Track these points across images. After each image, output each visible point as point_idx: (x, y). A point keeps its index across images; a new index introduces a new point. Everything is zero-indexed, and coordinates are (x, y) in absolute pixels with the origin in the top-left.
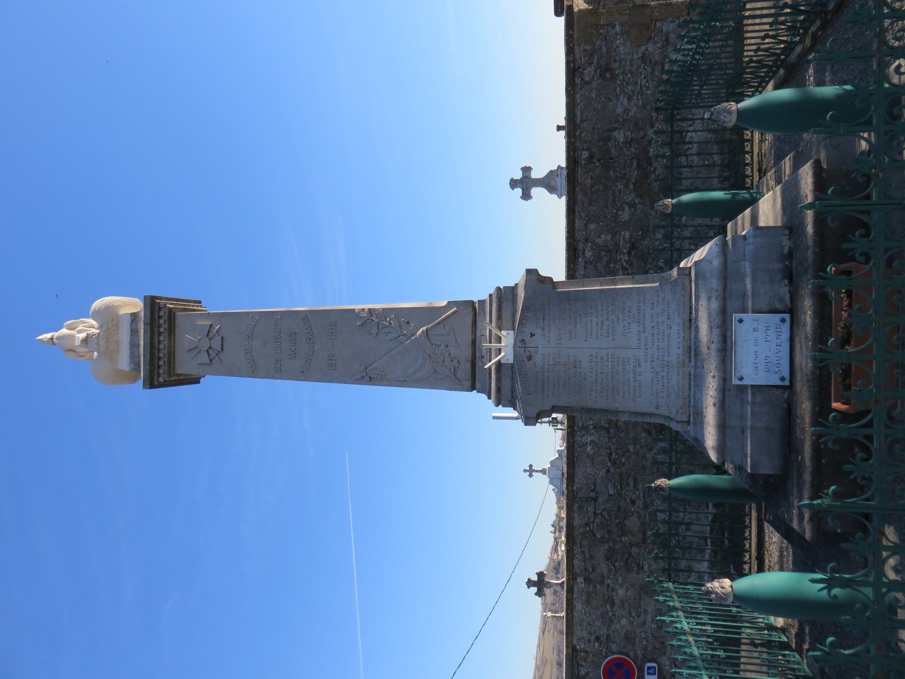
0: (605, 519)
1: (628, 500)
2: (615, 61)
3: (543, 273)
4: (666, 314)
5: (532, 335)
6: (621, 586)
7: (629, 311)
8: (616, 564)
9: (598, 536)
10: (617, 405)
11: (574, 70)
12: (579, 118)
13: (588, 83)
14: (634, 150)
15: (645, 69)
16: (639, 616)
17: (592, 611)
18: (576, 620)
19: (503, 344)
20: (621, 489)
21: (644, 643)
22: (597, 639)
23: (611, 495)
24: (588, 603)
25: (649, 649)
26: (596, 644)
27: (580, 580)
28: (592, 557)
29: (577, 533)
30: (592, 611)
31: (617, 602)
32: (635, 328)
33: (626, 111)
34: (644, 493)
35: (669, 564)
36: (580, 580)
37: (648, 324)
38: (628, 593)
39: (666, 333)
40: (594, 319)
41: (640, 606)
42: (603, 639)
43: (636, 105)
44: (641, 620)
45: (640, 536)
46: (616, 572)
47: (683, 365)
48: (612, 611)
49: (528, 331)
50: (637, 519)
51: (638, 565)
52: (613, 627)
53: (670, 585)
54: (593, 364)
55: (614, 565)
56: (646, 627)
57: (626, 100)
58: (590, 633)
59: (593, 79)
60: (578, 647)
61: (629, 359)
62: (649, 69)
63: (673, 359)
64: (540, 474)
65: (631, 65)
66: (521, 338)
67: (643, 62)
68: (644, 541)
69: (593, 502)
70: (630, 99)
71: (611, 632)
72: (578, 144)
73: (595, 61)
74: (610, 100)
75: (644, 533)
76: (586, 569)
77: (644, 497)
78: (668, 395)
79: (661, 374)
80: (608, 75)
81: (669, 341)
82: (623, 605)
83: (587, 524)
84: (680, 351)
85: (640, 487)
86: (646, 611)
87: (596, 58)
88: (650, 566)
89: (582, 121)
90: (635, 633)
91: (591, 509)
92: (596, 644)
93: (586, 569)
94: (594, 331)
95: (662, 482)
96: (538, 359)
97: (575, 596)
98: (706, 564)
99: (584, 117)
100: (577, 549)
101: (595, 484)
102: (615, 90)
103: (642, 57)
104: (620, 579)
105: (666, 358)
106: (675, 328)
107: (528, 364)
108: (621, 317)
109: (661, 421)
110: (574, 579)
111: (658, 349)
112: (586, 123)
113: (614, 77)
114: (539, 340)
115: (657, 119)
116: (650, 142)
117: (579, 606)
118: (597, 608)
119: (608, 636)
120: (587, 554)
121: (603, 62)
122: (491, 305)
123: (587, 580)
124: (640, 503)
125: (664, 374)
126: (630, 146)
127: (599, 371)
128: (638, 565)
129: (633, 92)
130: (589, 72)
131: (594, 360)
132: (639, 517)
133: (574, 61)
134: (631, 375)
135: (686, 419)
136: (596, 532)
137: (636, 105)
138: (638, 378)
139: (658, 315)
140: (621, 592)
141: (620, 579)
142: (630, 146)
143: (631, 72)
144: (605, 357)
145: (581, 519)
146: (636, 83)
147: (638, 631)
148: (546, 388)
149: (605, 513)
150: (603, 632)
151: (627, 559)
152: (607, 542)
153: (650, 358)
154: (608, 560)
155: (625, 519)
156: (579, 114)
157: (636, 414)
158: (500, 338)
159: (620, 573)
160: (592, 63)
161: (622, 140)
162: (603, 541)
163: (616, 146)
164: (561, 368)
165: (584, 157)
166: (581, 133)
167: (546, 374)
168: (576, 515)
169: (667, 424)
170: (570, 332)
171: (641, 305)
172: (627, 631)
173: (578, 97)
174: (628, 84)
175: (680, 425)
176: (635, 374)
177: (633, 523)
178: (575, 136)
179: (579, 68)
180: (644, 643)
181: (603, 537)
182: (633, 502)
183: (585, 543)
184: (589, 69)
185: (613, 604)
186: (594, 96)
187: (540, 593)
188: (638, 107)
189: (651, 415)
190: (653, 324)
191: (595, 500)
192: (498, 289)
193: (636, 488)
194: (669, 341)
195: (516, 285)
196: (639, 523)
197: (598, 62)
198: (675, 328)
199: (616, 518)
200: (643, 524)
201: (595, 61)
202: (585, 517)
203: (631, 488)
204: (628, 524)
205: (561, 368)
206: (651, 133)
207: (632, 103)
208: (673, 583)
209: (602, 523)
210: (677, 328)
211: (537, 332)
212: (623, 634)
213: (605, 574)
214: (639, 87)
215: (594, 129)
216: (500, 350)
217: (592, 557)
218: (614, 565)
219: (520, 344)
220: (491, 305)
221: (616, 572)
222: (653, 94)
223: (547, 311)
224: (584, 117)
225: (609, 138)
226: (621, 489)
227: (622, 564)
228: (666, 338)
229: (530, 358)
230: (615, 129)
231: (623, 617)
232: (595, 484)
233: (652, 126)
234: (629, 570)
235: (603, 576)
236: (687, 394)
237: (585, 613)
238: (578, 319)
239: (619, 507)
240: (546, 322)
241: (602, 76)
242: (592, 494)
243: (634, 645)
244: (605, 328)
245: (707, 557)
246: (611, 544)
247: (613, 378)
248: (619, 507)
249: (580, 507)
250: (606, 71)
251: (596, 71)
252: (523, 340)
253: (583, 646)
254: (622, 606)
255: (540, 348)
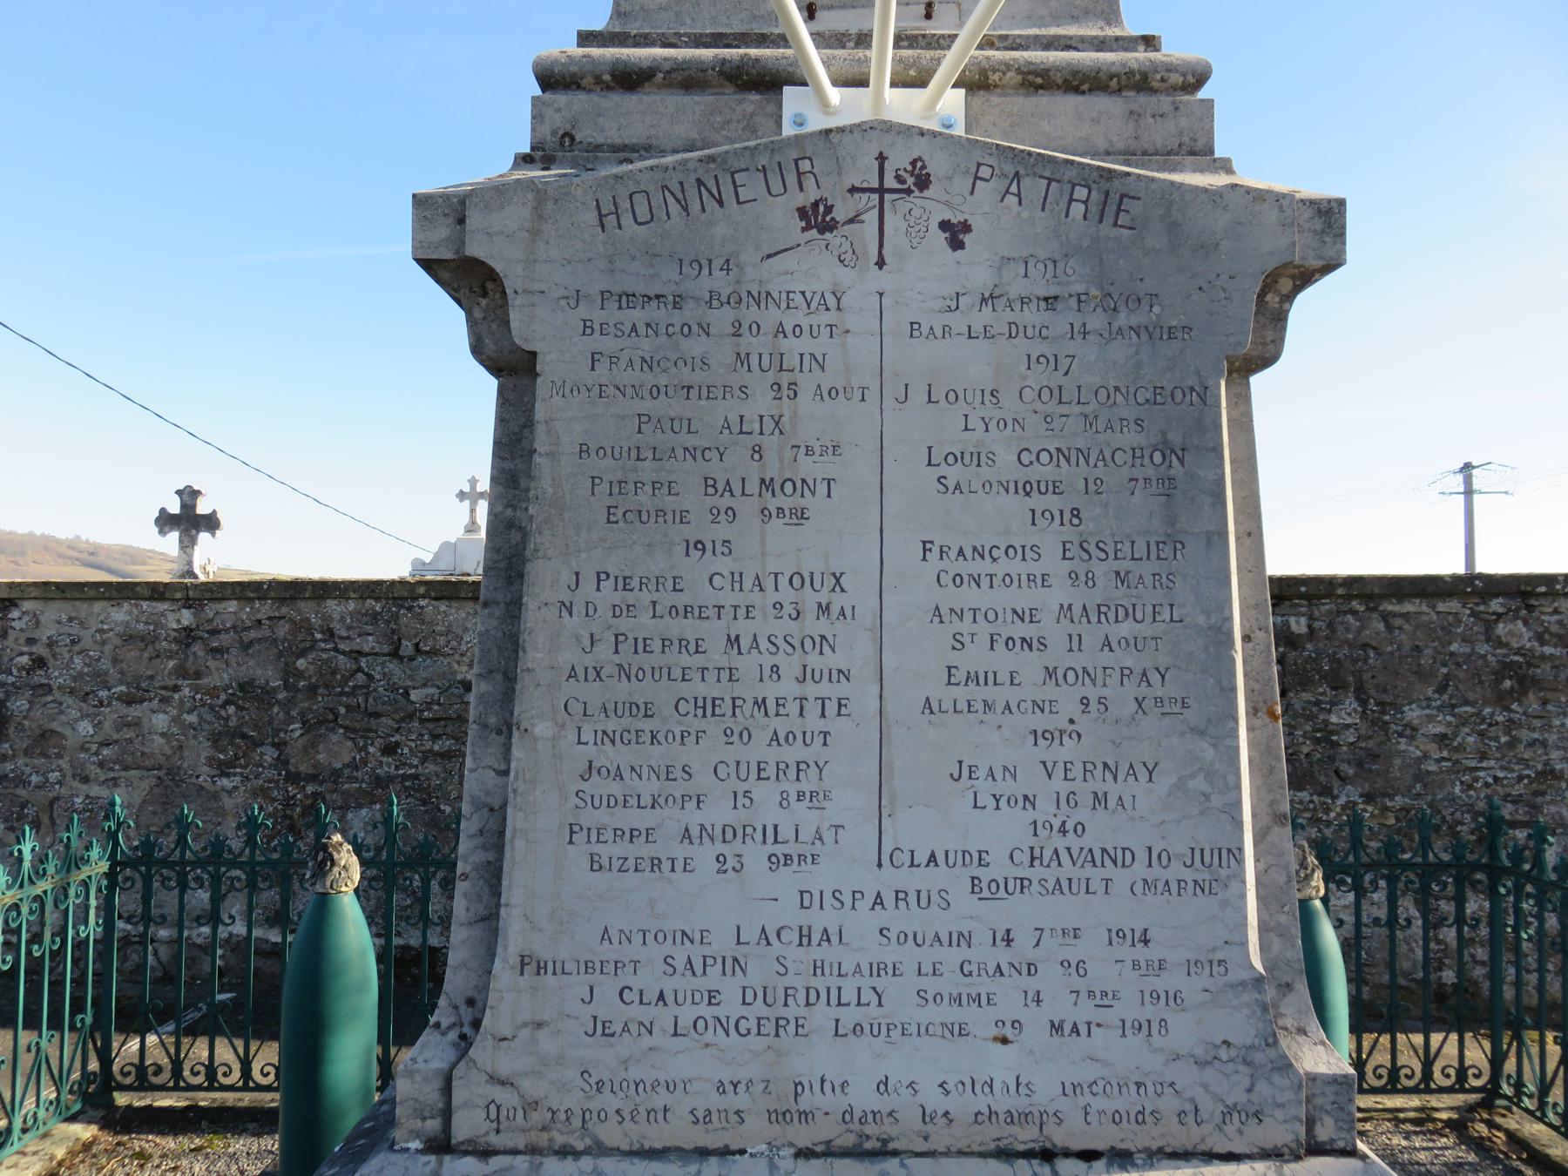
0: (346, 680)
1: (397, 737)
2: (1545, 703)
3: (1309, 310)
4: (1087, 1011)
5: (955, 234)
6: (176, 720)
7: (1099, 800)
8: (231, 709)
9: (301, 663)
10: (542, 729)
11: (1525, 595)
12: (1397, 608)
13: (1489, 627)
14: (1305, 750)
15: (1520, 778)
16: (101, 765)
17: (108, 648)
18: (83, 609)
19: (890, 94)
20: (422, 721)
21: (35, 779)
22: (39, 662)
23: (407, 694)
24: (129, 638)
25: (21, 792)
26: (25, 659)
27: (187, 617)
28: (246, 647)
29: (307, 609)
30: (108, 648)
31: (134, 712)
32: (1002, 833)
33: (1411, 732)
34: (415, 777)
35: (164, 863)
36: (187, 617)
37: (1022, 912)
38: (159, 740)
39: (969, 1014)
40: (1060, 594)
41: (126, 768)
42: (39, 678)
43: (1426, 756)
44: (93, 770)
45: (304, 768)
46: (212, 708)
47: (780, 1116)
48: (110, 698)
49: (979, 205)
50: (347, 760)
51: (231, 764)
52: (69, 701)
53: (98, 865)
54: (787, 595)
55: (227, 702)
56: (76, 784)
57: (1440, 729)
58: (51, 644)
59: (1500, 643)
60: (15, 614)
61: (813, 798)
62: (1518, 789)
63: (815, 1057)
64: (466, 520)
65: (1531, 744)
66: (937, 166)
67: (1538, 773)
68: (294, 778)
69: (386, 649)
70: (1441, 739)
71: (57, 695)
72: (1327, 606)
73: (1548, 650)
74: (1442, 689)
75: (312, 778)
76: (214, 632)
77: (405, 777)
78: (602, 1029)
79: (730, 990)
80: (1508, 684)
81: (924, 1031)
82: (129, 725)
83: (330, 634)
84: (863, 1097)
85: (431, 768)
86: (115, 782)
87: (1557, 652)
88: (229, 792)
89: (1386, 617)
90: (59, 756)
91: (369, 644)
92: (25, 659)
93: (214, 632)
94: (969, 596)
95: (349, 868)
96: (812, 268)
97: (145, 605)
98: (240, 929)
99: (1398, 622)
100: (264, 609)
101: (434, 652)
102: (1467, 703)
103: (1552, 771)
104: (192, 718)
105: (821, 1016)
106: (1001, 1064)
107: (780, 215)
108: (1067, 750)
109: (456, 981)
110: (188, 603)
111: (878, 969)
112: (1381, 626)
113: (1502, 700)
114: (925, 272)
115: (1385, 809)
116: (1327, 791)
117: (120, 615)
118: (115, 661)
119: (47, 689)
120: (253, 634)
121: (1543, 671)
122: (1101, 44)
123: (187, 636)
124: (388, 766)
125: (730, 1007)
126: (1317, 741)
127: (744, 628)
128: (231, 764)
129: (1461, 748)
130: (1516, 633)
131: (810, 599)
132: (354, 765)
133: (1553, 594)
134: (719, 813)
135: (465, 1126)
136: (311, 656)
137: (1426, 756)
138: (704, 855)
139: (1080, 967)
140: (161, 721)
141: (192, 718)
142: (1317, 741)
143: (1512, 744)
144: (832, 660)
145: (342, 619)
146: (1483, 756)
147: (64, 763)
148: (637, 315)
149: (360, 678)
150: (58, 676)
151: (244, 736)
152: (286, 686)
153: (819, 920)
154: (241, 687)
155: (346, 728)
156: (1408, 607)
157: (496, 840)
158: (921, 82)
159: (209, 717)
160: (1543, 643)
161: (1334, 719)
162: (289, 673)
163: (1318, 703)
164: (762, 403)
165: (1292, 620)
166: (1354, 613)
167: (722, 318)
168: (352, 605)
169: (442, 1014)
170: (977, 458)
171: (1140, 870)
172: (63, 737)
173: (1453, 605)
174: (1482, 734)
175: (431, 1094)
176: (730, 833)
177: (337, 750)
178: (1349, 597)
179: (1530, 608)
180: (35, 779)
181: (300, 674)
182: (390, 750)
183: (283, 630)
184: (1527, 634)
185: (129, 700)
186: (1454, 647)
187: (165, 521)
188: (1420, 761)
189: (490, 920)
190: (1024, 938)
191: (395, 654)
192: (1197, 77)
193: (427, 756)
194: (924, 1031)
195: (1225, 166)
196: (338, 765)
197: (1543, 657)
198: (1001, 1064)
199: (348, 707)
200: (336, 774)
201: (1548, 650)
202: (349, 628)
203: (428, 745)
204: (334, 738)
205: (762, 403)
206: (1349, 794)
207: (1432, 749)
208: (111, 875)
209: (334, 672)
210: (1004, 1076)
211: (975, 268)
212: (54, 726)
213: (205, 681)
214: (1473, 764)
215: (1365, 646)
216: (862, 82)
217: (246, 647)
218: (227, 702)
219: (899, 160)
220: (1101, 44)
221: (212, 708)
222: (1452, 799)
223: (1096, 321)
224: (1398, 622)
225: (1338, 685)
226: (422, 721)
227: (233, 723)
228: (952, 1014)
229: (817, 218)
230: (1363, 703)
231: (98, 726)
232: (434, 652)
233: (1369, 798)
234: (215, 739)
235: (198, 675)
236: (611, 1134)
237: (100, 631)
238: (1053, 502)
239: (377, 715)
240: (1032, 316)
241: (1506, 668)
242: (407, 647)
243: (26, 752)
244: (1004, 661)
245: (257, 933)
246: (281, 696)
247: (707, 707)
248: (377, 715)
249: (375, 616)
250: (1518, 678)
251: (1518, 652)
252: (923, 182)
253: (17, 625)
254: (123, 724)
255: (877, 279)
